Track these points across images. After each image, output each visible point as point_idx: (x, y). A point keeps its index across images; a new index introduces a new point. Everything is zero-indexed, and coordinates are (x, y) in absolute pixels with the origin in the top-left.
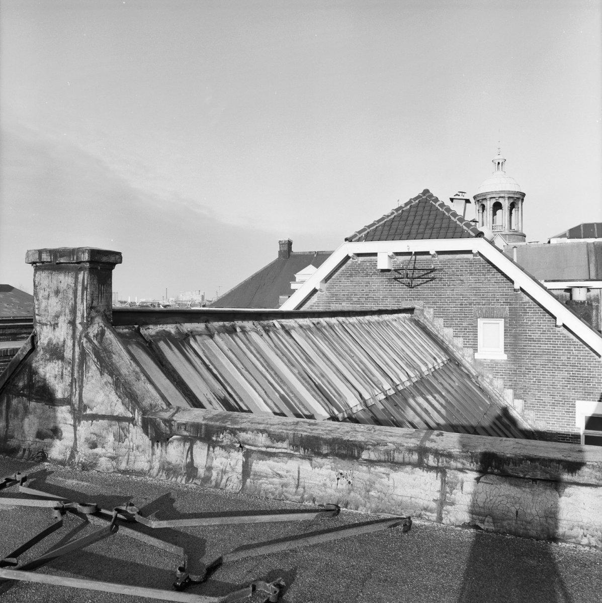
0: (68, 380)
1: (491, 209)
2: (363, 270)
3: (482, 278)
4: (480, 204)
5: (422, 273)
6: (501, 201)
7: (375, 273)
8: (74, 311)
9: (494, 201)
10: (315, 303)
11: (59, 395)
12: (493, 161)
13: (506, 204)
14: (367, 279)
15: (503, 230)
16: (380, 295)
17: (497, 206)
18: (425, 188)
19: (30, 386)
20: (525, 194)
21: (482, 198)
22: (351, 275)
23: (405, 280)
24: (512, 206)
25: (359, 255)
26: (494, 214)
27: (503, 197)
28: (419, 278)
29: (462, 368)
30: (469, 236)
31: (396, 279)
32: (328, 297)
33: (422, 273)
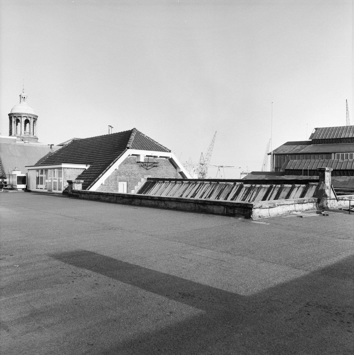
0: (329, 193)
1: (24, 123)
2: (130, 161)
3: (168, 167)
4: (16, 118)
5: (151, 164)
6: (29, 119)
7: (134, 163)
8: (330, 180)
9: (25, 118)
10: (110, 176)
11: (328, 196)
12: (24, 98)
13: (32, 121)
14: (131, 165)
15: (30, 135)
16: (136, 172)
17: (27, 121)
18: (135, 127)
19: (325, 195)
20: (38, 116)
21: (18, 115)
22: (125, 163)
23: (145, 167)
24: (34, 122)
25: (133, 155)
26: (17, 125)
27: (30, 117)
28: (149, 166)
29: (236, 196)
30: (168, 152)
31: (142, 166)
32: (116, 173)
33: (151, 164)
